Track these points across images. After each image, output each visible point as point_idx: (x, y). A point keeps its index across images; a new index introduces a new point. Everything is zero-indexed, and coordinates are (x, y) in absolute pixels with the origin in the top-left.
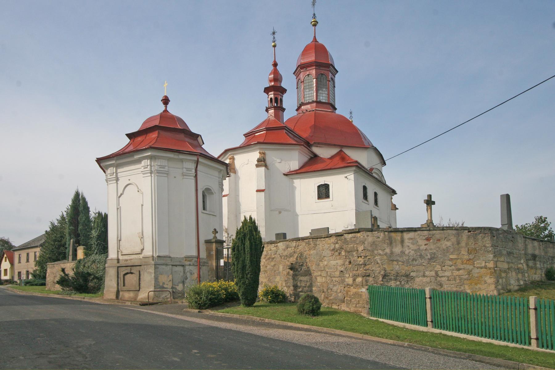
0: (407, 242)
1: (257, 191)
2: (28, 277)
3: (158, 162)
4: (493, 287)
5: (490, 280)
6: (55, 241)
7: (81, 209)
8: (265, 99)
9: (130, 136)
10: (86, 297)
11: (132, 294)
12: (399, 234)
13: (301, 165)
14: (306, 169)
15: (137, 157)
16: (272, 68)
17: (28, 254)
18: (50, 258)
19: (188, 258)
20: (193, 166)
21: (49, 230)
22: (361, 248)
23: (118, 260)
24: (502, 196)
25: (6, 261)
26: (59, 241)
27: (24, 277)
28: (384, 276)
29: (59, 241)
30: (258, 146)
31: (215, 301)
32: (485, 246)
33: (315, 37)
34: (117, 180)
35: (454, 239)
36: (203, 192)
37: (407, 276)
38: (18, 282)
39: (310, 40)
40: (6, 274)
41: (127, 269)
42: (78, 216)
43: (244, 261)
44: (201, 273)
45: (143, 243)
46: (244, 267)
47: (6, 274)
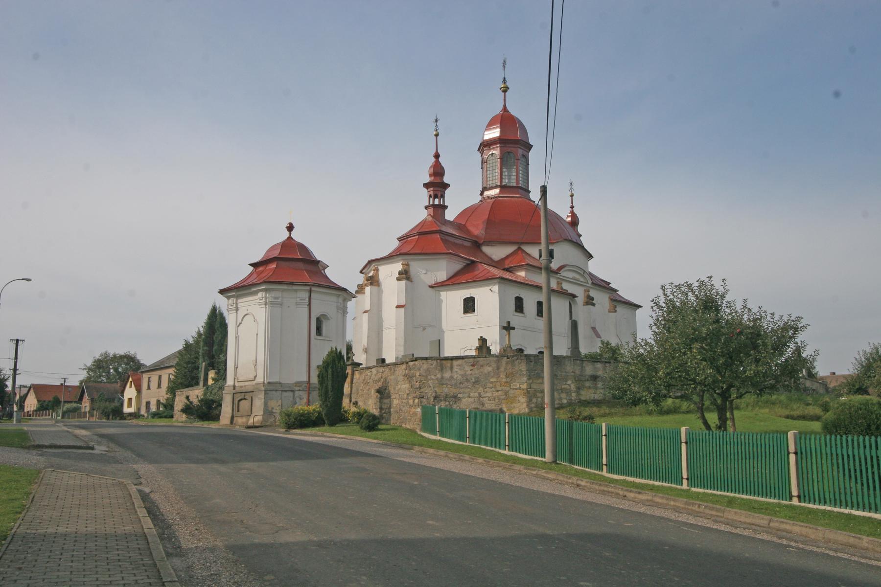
0: (455, 369)
1: (398, 307)
2: (158, 408)
3: (273, 294)
4: (525, 405)
5: (523, 400)
6: (188, 363)
7: (217, 325)
8: (423, 196)
9: (254, 265)
11: (244, 420)
12: (450, 362)
13: (451, 274)
14: (452, 282)
15: (253, 290)
16: (434, 160)
17: (160, 377)
18: (181, 384)
19: (298, 384)
20: (307, 295)
22: (418, 374)
23: (234, 387)
24: (431, 342)
25: (131, 387)
26: (193, 363)
27: (153, 408)
28: (435, 398)
29: (193, 363)
30: (401, 258)
31: (304, 422)
32: (521, 371)
33: (505, 105)
34: (237, 309)
35: (494, 365)
36: (318, 319)
37: (455, 397)
38: (146, 415)
39: (498, 110)
40: (130, 405)
41: (242, 396)
42: (214, 334)
43: (326, 387)
44: (311, 398)
45: (256, 370)
46: (326, 392)
47: (130, 405)
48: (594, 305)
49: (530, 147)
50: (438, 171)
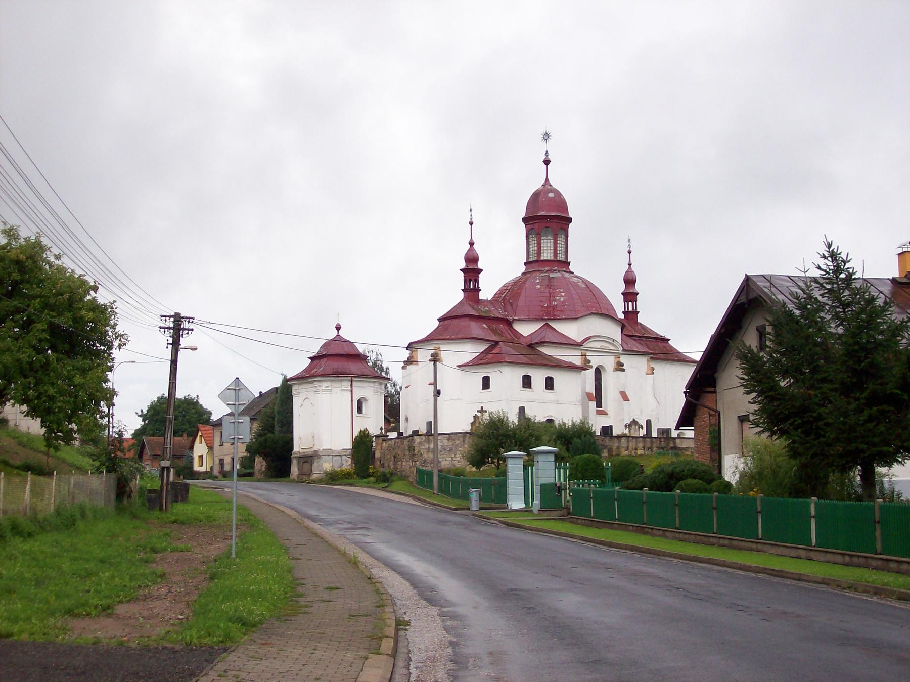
9: (312, 359)
10: (900, 251)
20: (349, 384)
21: (110, 375)
33: (547, 180)
35: (461, 439)
48: (623, 370)
49: (570, 220)
50: (472, 259)
